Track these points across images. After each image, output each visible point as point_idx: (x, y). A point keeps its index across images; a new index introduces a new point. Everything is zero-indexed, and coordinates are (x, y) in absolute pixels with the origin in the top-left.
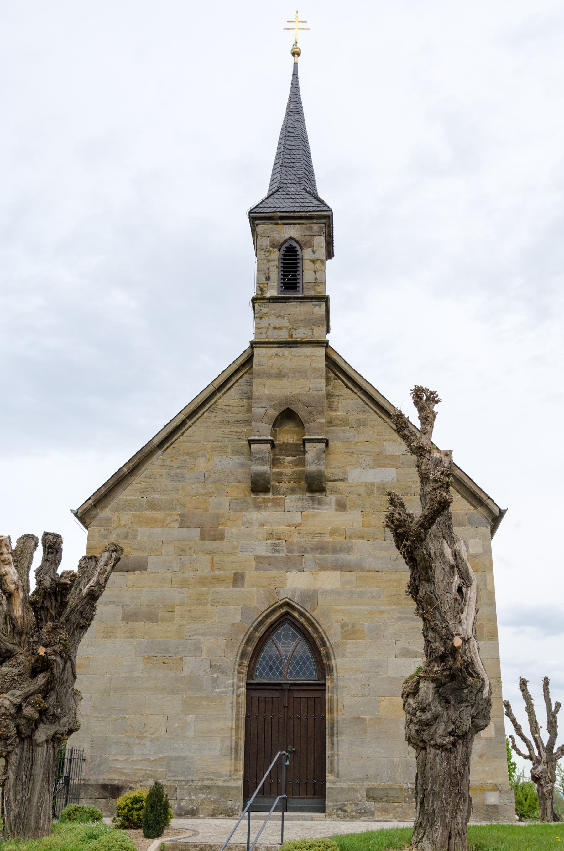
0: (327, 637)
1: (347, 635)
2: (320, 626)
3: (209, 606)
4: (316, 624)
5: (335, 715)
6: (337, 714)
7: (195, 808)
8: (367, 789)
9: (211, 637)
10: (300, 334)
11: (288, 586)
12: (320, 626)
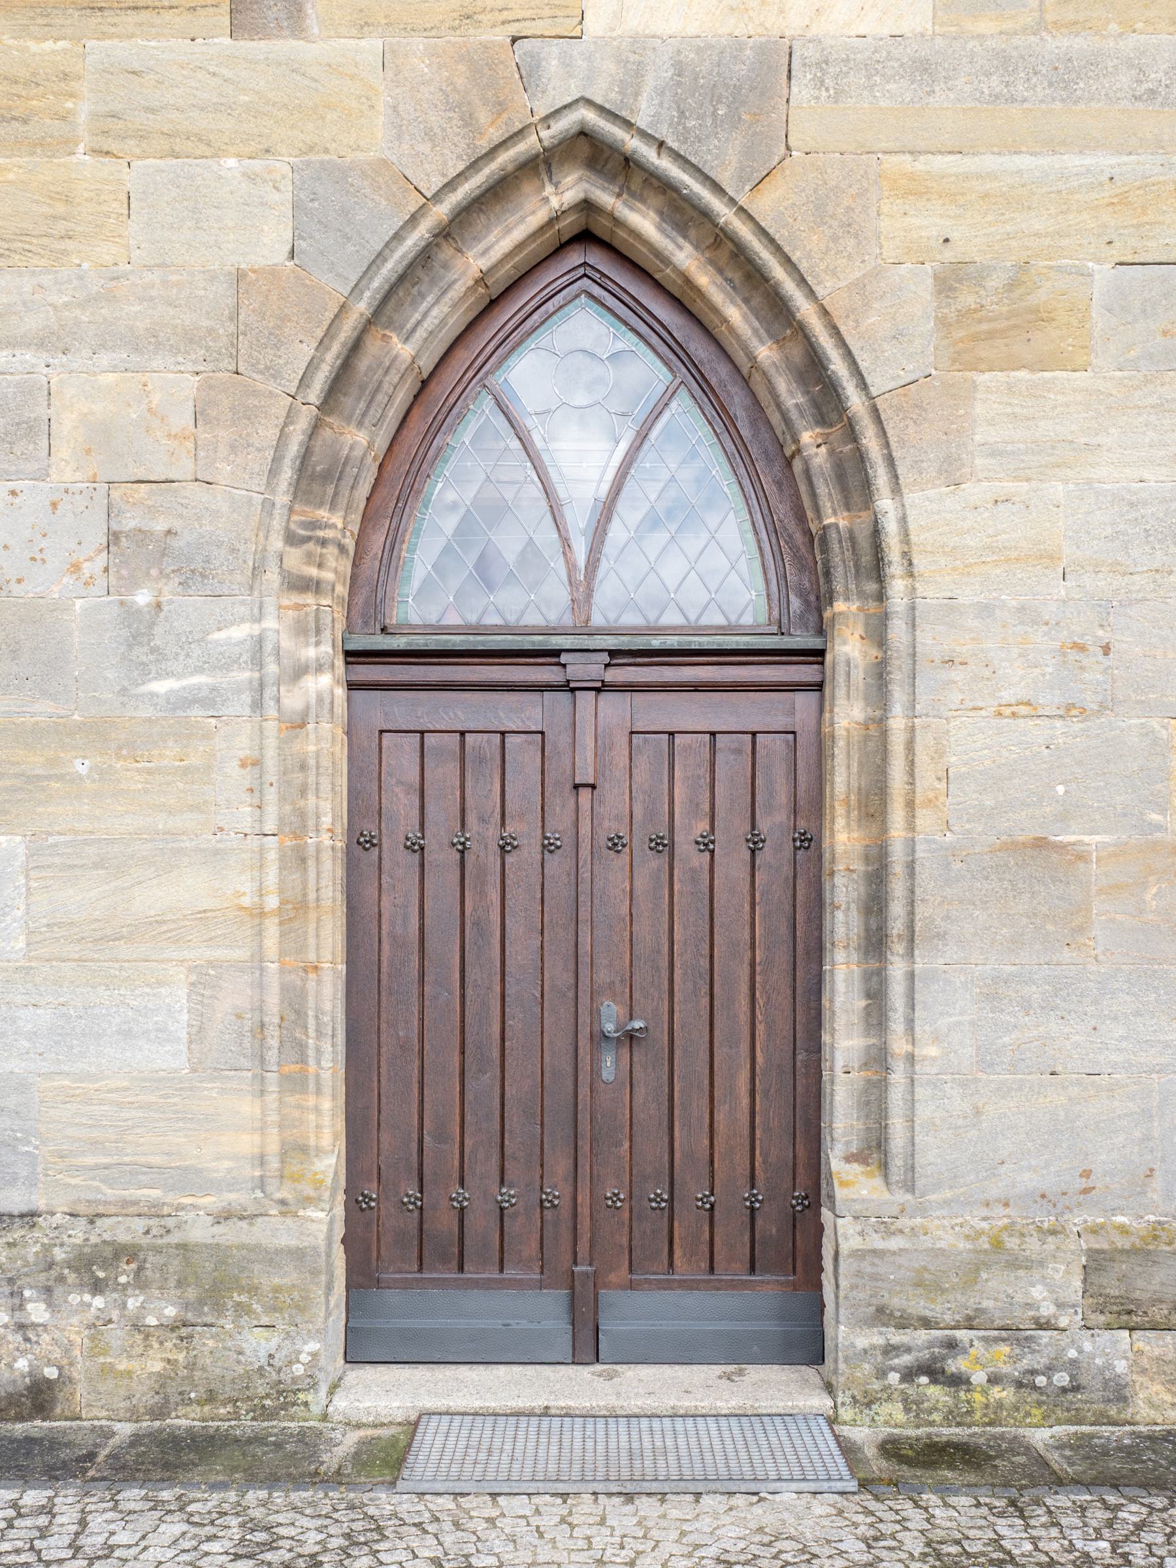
0: (849, 355)
1: (975, 338)
2: (802, 281)
3: (80, 156)
4: (778, 272)
5: (897, 830)
6: (911, 826)
7: (51, 1373)
8: (1092, 1254)
9: (104, 359)
11: (594, 26)
12: (802, 281)
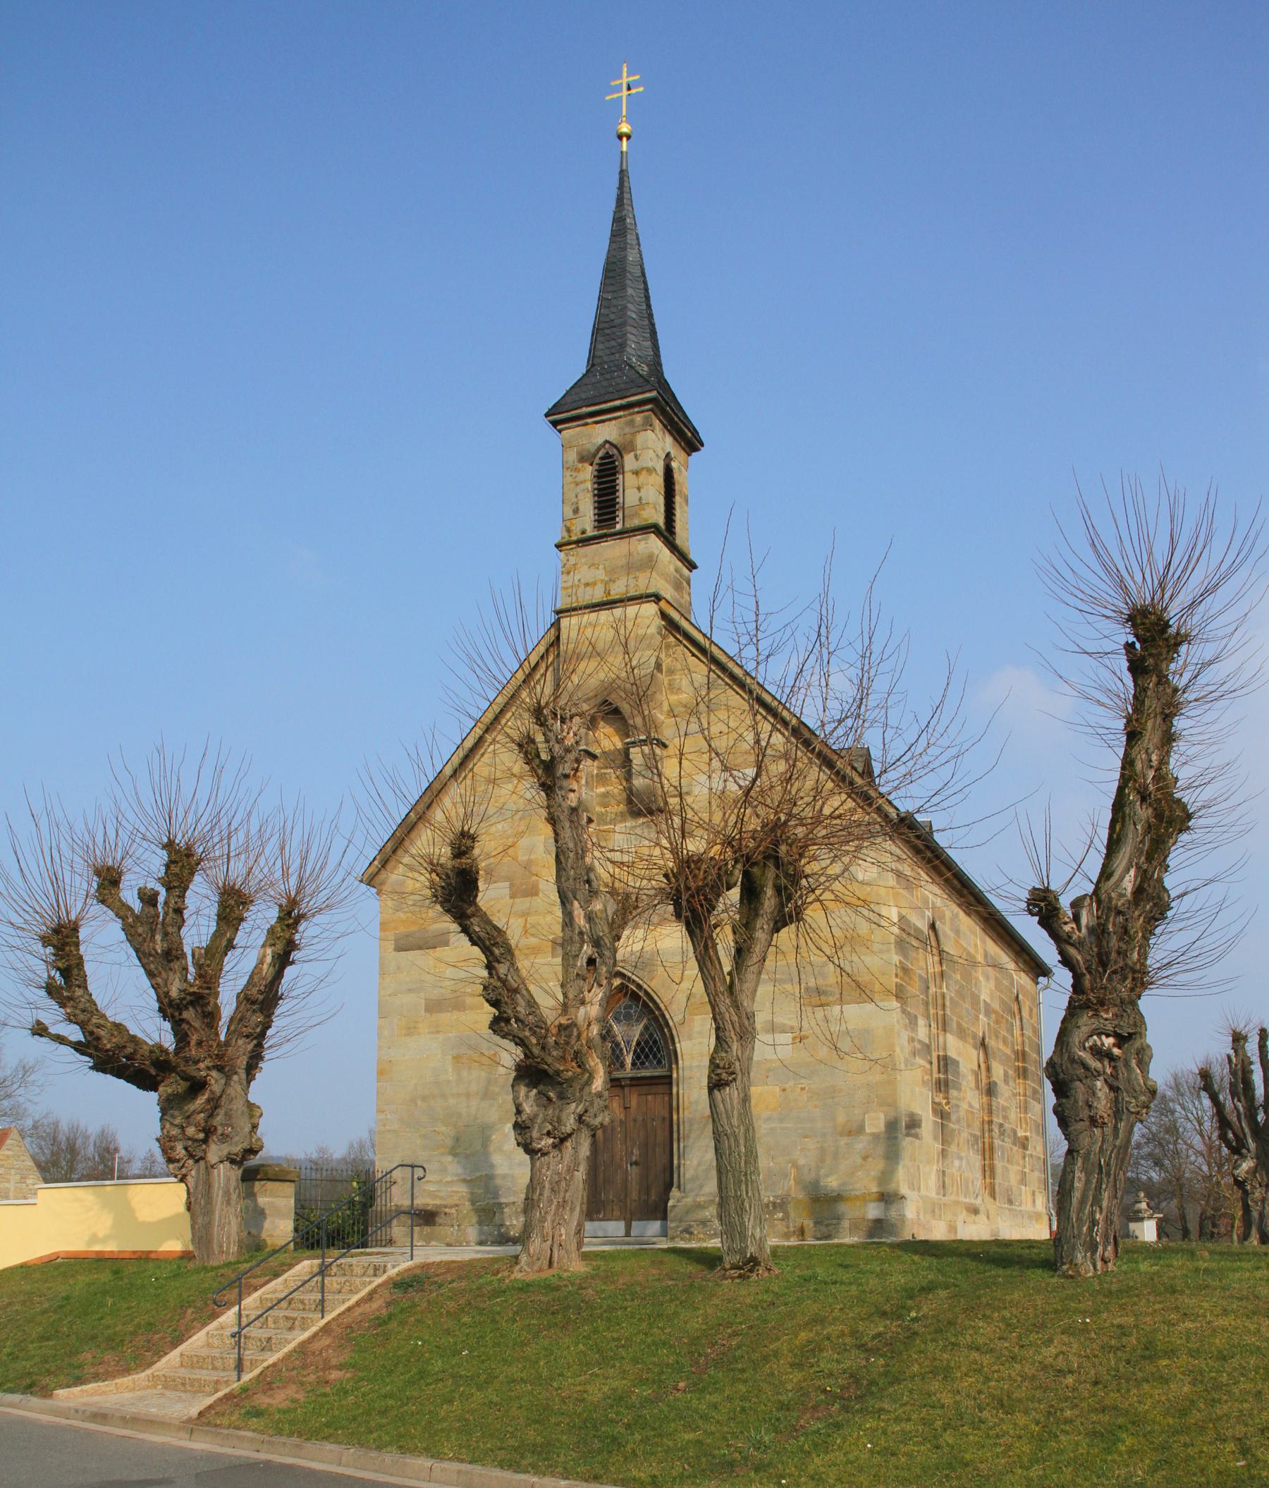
10: (618, 590)
